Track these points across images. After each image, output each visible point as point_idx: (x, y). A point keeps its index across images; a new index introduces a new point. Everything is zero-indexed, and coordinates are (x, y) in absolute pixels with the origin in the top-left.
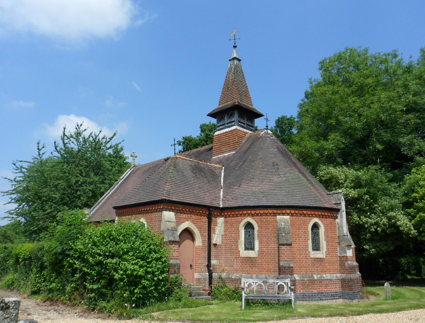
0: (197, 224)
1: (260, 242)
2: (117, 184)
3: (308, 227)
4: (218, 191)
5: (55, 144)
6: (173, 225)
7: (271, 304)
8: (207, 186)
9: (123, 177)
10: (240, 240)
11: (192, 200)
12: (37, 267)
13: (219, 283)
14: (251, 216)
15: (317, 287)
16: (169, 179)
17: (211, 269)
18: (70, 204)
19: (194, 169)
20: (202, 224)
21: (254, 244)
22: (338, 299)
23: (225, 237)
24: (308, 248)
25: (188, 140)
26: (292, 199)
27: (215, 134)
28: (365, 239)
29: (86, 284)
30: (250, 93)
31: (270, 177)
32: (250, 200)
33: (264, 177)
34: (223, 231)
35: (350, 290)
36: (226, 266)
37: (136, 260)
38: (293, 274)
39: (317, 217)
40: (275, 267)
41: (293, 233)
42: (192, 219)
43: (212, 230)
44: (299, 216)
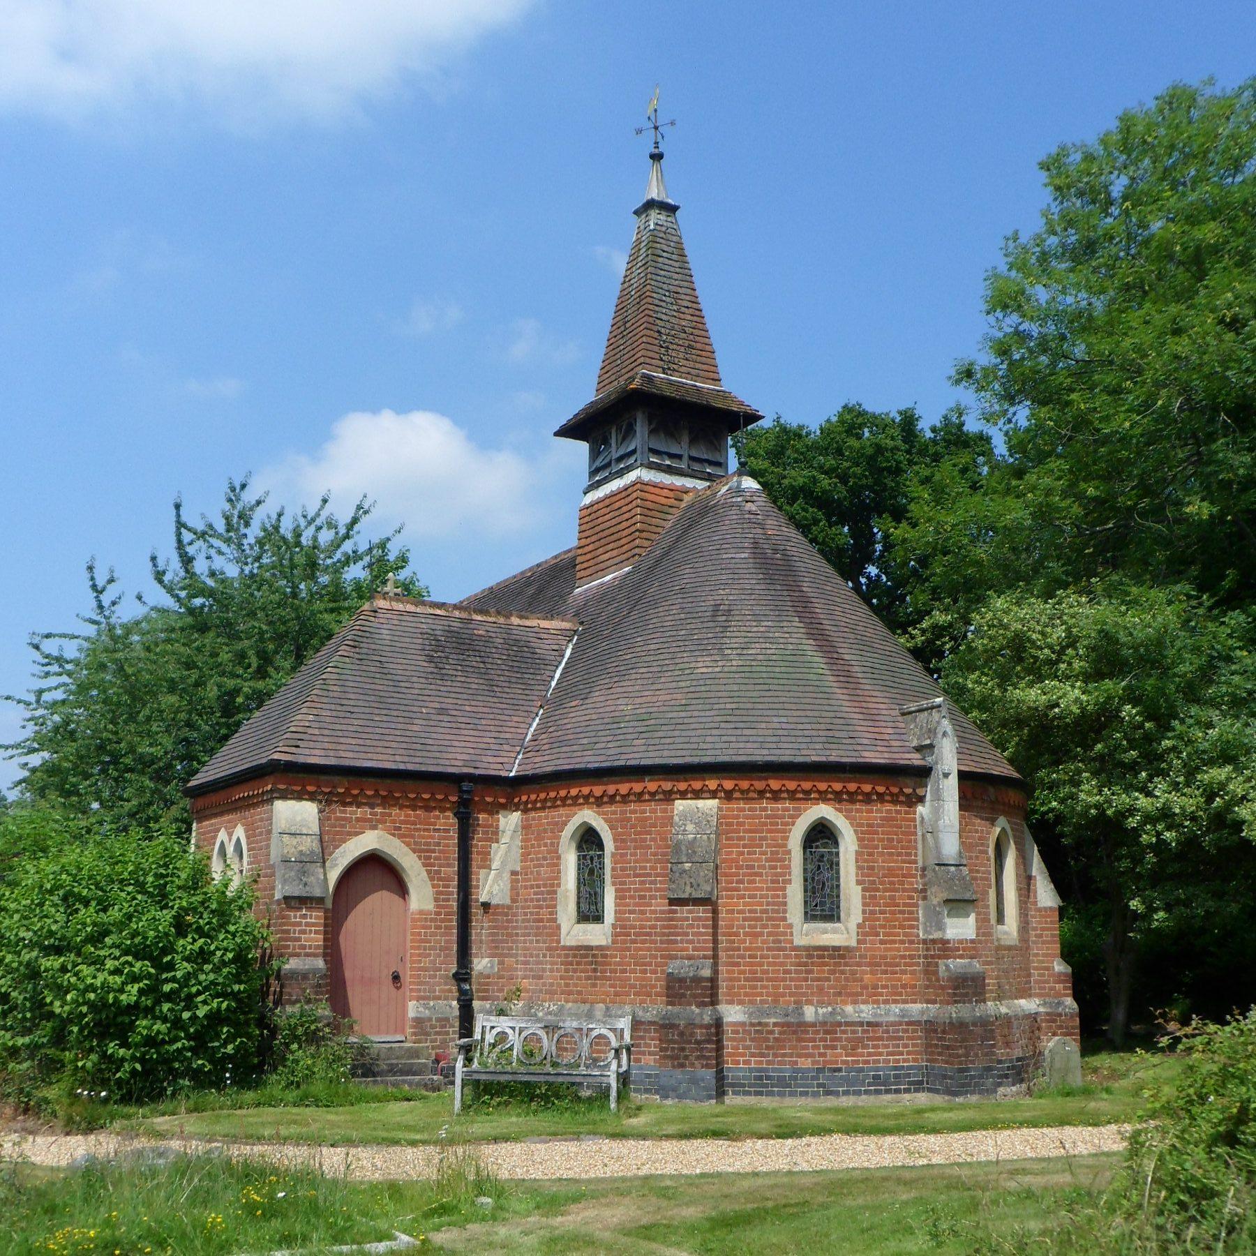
0: (412, 837)
1: (620, 897)
3: (787, 838)
5: (155, 565)
19: (439, 646)
20: (433, 837)
22: (907, 1091)
24: (785, 911)
30: (711, 333)
31: (686, 660)
34: (518, 857)
42: (394, 822)
43: (474, 856)
44: (800, 799)
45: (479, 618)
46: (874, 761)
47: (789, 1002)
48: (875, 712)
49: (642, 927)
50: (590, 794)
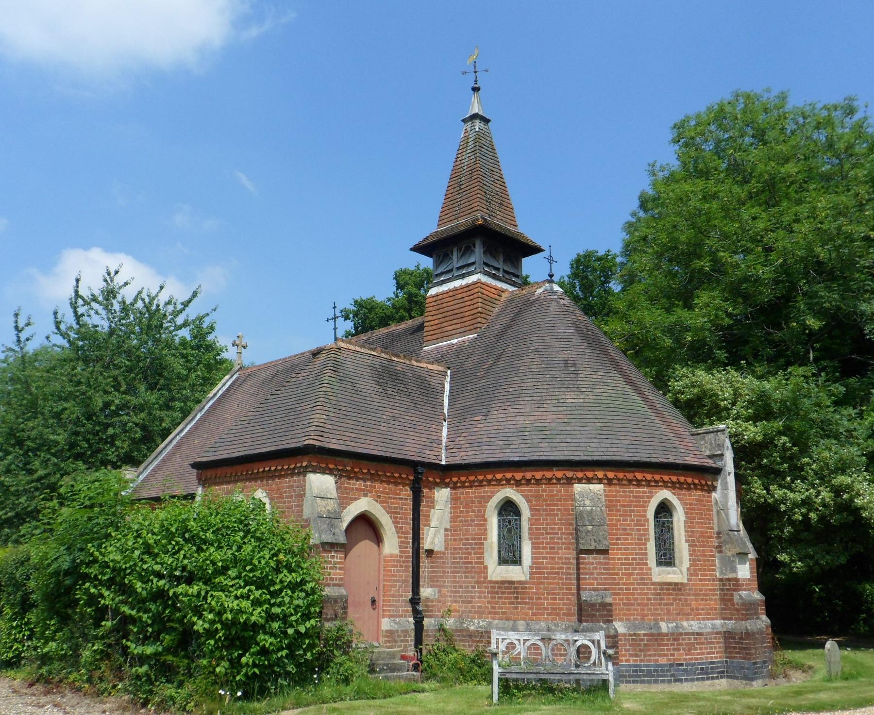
0: (387, 503)
1: (535, 547)
2: (200, 411)
3: (646, 511)
4: (436, 427)
5: (56, 318)
6: (332, 505)
7: (561, 691)
8: (409, 414)
9: (215, 395)
10: (489, 541)
11: (376, 448)
12: (13, 605)
13: (438, 640)
14: (513, 484)
15: (668, 650)
16: (321, 399)
17: (420, 608)
18: (91, 456)
19: (380, 376)
20: (398, 504)
21: (520, 551)
22: (717, 678)
23: (452, 535)
24: (646, 559)
25: (366, 308)
26: (608, 445)
27: (429, 294)
28: (780, 539)
29: (129, 644)
31: (557, 393)
32: (511, 446)
33: (544, 394)
35: (744, 658)
36: (456, 602)
37: (244, 587)
38: (610, 621)
39: (667, 487)
40: (570, 604)
41: (613, 525)
42: (376, 491)
43: (421, 517)
44: (652, 486)
45: (396, 359)
46: (693, 463)
47: (650, 620)
48: (678, 432)
49: (552, 568)
50: (513, 478)
